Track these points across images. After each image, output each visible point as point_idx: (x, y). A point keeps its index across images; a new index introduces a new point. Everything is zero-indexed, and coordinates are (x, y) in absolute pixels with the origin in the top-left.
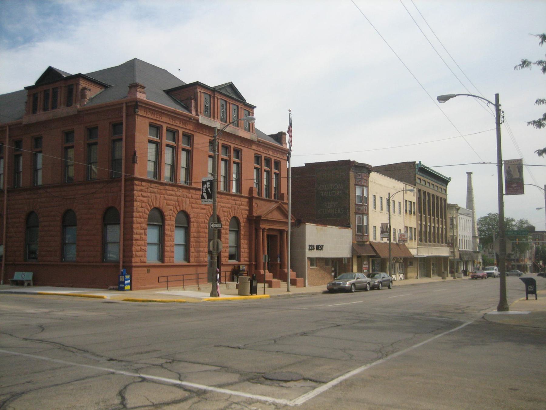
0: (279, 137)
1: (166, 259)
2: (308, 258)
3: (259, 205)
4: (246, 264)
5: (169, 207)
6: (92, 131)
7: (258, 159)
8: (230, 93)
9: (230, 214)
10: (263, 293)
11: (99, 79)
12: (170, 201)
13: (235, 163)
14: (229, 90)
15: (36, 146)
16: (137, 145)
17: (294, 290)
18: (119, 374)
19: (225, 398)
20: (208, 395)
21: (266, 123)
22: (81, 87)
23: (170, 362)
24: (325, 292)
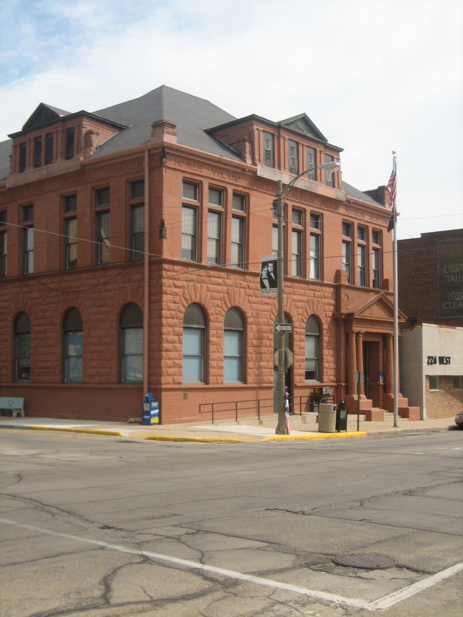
0: (378, 194)
1: (212, 379)
2: (427, 376)
3: (350, 296)
4: (331, 386)
5: (215, 301)
6: (101, 193)
7: (347, 227)
8: (303, 131)
9: (306, 311)
10: (357, 429)
11: (111, 118)
12: (215, 293)
13: (312, 234)
14: (301, 125)
15: (26, 218)
16: (165, 210)
17: (404, 424)
18: (112, 550)
19: (266, 594)
20: (240, 588)
21: (359, 173)
22: (84, 131)
23: (193, 534)
24: (452, 429)
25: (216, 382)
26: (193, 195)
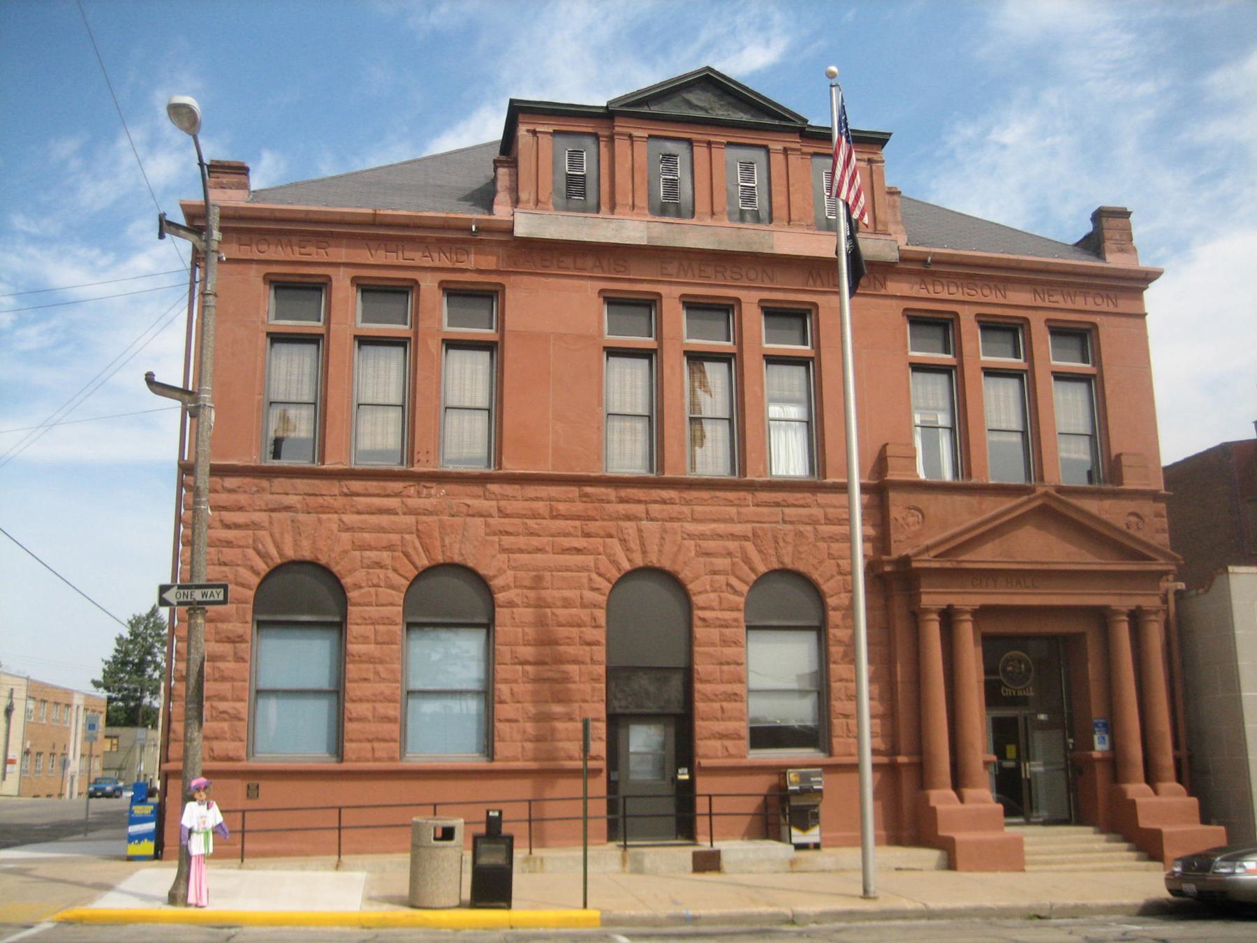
25: (369, 755)
26: (1009, 348)
